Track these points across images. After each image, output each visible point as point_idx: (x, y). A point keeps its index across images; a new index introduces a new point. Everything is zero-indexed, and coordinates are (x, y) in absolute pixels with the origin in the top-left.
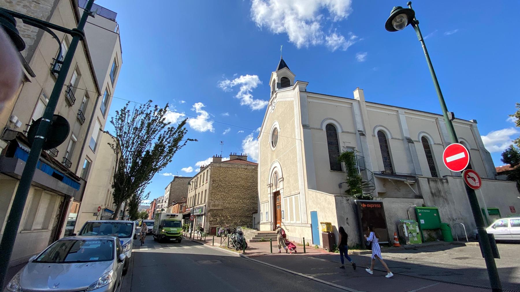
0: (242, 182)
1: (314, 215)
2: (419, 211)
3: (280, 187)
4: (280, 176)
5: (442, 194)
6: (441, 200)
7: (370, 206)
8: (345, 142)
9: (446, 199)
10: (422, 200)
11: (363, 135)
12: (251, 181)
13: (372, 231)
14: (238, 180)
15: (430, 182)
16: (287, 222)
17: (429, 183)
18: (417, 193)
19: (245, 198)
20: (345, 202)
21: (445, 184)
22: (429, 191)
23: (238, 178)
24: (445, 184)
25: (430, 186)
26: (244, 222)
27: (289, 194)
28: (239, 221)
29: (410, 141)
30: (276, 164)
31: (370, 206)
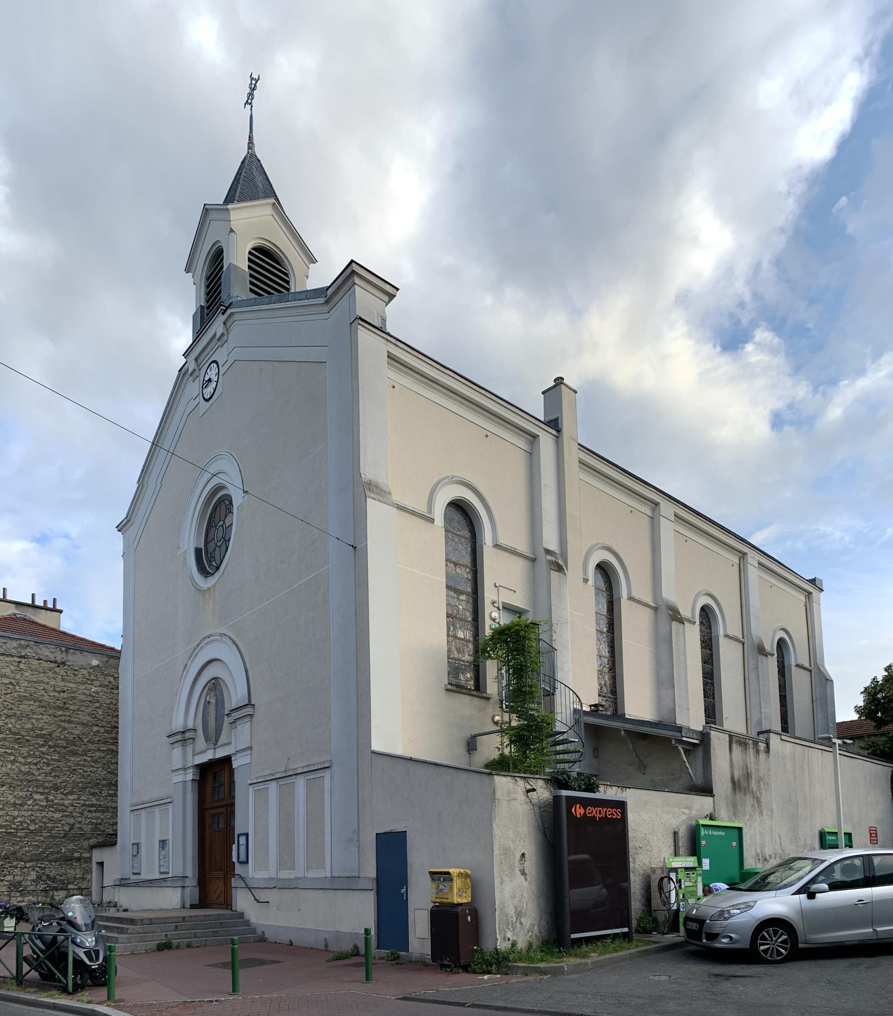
0: (44, 722)
1: (392, 849)
2: (703, 832)
3: (236, 742)
4: (236, 694)
5: (753, 785)
6: (749, 800)
7: (593, 812)
8: (505, 585)
9: (758, 801)
10: (711, 799)
11: (559, 569)
12: (85, 718)
13: (96, 942)
14: (24, 707)
15: (734, 746)
16: (262, 875)
17: (730, 750)
18: (699, 781)
19: (56, 788)
20: (521, 797)
21: (762, 756)
22: (729, 776)
23: (21, 699)
24: (762, 756)
25: (731, 760)
26: (53, 880)
27: (279, 770)
28: (33, 875)
29: (675, 616)
30: (220, 650)
31: (593, 812)
